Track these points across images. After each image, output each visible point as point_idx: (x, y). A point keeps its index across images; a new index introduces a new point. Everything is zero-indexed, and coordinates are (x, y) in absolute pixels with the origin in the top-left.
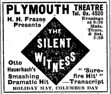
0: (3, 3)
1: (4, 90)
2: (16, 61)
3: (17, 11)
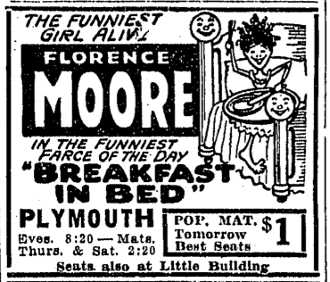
0: (305, 255)
1: (9, 265)
2: (145, 236)
3: (43, 222)
